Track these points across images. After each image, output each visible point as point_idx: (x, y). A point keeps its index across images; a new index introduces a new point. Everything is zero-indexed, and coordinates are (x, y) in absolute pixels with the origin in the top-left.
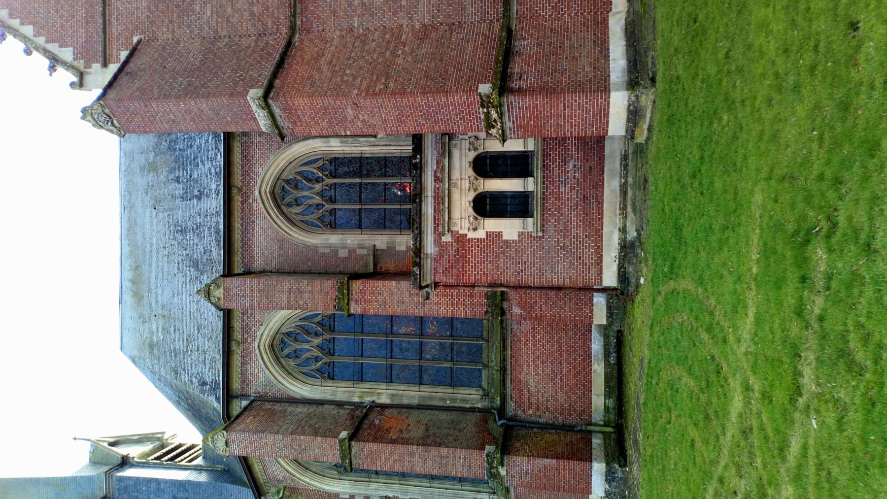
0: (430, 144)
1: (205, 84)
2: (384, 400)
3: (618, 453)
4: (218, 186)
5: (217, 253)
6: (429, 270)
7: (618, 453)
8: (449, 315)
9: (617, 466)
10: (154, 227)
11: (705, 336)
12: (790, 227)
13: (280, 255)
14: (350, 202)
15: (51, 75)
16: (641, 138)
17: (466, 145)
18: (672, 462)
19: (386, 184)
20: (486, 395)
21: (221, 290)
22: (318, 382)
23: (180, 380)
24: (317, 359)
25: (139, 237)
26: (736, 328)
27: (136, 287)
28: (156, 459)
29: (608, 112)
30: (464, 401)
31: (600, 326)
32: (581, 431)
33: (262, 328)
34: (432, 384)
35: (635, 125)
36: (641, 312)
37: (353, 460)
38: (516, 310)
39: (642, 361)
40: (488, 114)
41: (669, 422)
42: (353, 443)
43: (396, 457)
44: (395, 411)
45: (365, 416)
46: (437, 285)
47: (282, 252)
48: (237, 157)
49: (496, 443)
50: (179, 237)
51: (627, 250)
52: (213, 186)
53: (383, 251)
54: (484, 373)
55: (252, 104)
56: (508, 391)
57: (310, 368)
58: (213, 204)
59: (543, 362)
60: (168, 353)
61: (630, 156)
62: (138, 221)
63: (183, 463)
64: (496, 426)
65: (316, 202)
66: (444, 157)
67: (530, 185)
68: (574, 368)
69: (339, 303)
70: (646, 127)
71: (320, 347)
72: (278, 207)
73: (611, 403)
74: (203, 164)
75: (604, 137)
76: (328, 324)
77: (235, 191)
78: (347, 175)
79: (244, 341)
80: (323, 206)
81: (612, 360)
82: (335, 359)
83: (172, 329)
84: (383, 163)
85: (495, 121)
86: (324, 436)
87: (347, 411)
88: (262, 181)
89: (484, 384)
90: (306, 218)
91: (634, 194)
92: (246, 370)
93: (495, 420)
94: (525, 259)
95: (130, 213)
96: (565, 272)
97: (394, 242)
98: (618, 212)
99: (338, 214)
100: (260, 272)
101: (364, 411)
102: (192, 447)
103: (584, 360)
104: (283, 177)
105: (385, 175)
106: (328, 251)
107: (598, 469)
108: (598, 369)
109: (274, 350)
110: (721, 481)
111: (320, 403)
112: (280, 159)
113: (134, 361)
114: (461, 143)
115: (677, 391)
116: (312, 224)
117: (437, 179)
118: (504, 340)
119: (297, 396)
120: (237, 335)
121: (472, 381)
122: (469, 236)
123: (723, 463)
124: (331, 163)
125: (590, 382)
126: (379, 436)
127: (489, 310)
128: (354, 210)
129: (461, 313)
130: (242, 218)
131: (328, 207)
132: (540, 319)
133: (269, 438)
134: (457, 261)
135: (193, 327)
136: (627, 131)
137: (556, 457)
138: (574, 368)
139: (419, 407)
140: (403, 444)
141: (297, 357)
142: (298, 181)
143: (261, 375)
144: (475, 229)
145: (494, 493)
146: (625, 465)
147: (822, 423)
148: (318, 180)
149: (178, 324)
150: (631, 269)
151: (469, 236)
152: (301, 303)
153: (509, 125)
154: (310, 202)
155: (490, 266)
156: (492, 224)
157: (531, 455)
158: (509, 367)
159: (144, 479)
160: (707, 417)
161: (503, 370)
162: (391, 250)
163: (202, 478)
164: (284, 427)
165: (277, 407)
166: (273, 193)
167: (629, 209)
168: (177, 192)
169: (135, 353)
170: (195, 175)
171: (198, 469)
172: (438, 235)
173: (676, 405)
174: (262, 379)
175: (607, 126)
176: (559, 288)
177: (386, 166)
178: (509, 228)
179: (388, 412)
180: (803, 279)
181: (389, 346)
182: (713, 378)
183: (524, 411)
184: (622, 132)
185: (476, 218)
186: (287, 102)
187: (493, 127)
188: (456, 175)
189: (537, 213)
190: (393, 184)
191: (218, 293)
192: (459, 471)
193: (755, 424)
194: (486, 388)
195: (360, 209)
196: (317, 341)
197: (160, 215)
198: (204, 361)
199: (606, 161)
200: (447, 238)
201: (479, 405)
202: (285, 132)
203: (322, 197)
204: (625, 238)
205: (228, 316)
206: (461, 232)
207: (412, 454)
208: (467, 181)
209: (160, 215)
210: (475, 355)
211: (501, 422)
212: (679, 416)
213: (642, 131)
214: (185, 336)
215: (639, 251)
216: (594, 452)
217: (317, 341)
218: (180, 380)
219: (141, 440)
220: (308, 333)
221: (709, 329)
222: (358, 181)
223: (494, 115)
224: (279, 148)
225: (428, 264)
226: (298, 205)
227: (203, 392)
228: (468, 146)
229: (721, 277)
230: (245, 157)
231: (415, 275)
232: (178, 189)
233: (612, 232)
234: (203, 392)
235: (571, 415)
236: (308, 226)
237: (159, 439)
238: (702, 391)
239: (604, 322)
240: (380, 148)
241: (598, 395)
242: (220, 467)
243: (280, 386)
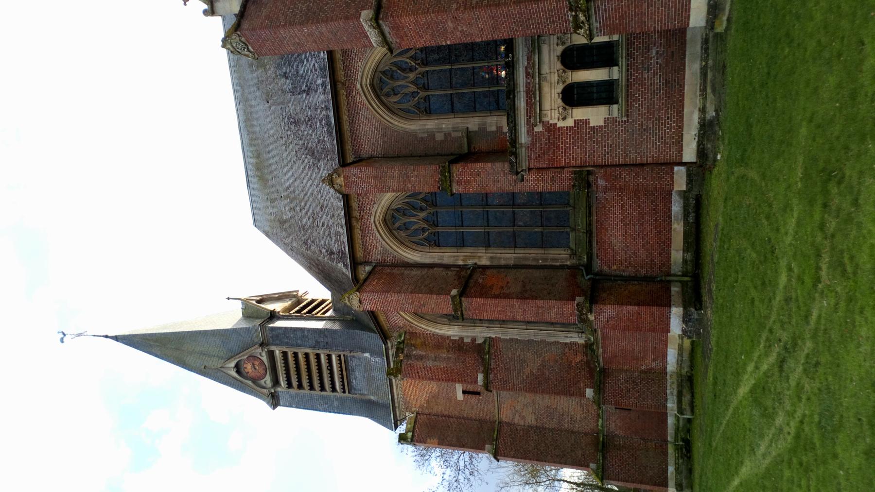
1: (322, 8)
2: (485, 262)
3: (694, 298)
4: (324, 82)
5: (331, 143)
7: (694, 298)
8: (540, 189)
9: (693, 310)
10: (269, 119)
11: (765, 221)
12: (821, 165)
13: (384, 142)
14: (441, 88)
15: (185, 4)
16: (720, 28)
17: (554, 39)
18: (738, 312)
19: (474, 68)
20: (574, 254)
21: (342, 178)
22: (427, 249)
23: (311, 251)
24: (424, 230)
25: (257, 128)
26: (785, 224)
27: (260, 171)
28: (296, 312)
29: (690, 7)
30: (553, 260)
31: (680, 193)
32: (661, 281)
33: (376, 206)
34: (525, 246)
35: (715, 17)
36: (717, 186)
38: (601, 182)
39: (717, 226)
40: (576, 17)
41: (736, 282)
42: (463, 299)
44: (495, 271)
45: (470, 276)
46: (530, 169)
49: (585, 295)
50: (294, 128)
51: (706, 128)
52: (319, 82)
53: (475, 132)
54: (572, 235)
55: (364, 25)
56: (595, 251)
58: (321, 98)
59: (626, 225)
60: (297, 229)
61: (711, 39)
62: (254, 114)
63: (319, 315)
64: (585, 280)
65: (411, 90)
66: (534, 53)
67: (615, 73)
68: (656, 228)
69: (442, 184)
70: (725, 18)
71: (425, 220)
72: (378, 97)
73: (689, 256)
74: (308, 61)
75: (686, 29)
76: (431, 200)
77: (339, 86)
78: (438, 62)
80: (418, 93)
81: (691, 219)
82: (439, 229)
83: (298, 208)
85: (583, 22)
86: (439, 294)
87: (454, 273)
89: (572, 245)
91: (714, 76)
92: (366, 242)
93: (583, 275)
94: (610, 142)
95: (245, 105)
96: (648, 151)
97: (485, 124)
98: (698, 93)
99: (432, 100)
100: (369, 158)
101: (469, 272)
102: (323, 301)
103: (664, 221)
104: (381, 68)
105: (472, 60)
107: (676, 314)
108: (678, 228)
110: (771, 331)
111: (431, 266)
113: (267, 235)
115: (743, 259)
116: (409, 111)
117: (528, 75)
118: (589, 207)
119: (411, 261)
120: (356, 213)
122: (558, 125)
123: (773, 319)
125: (670, 239)
126: (484, 292)
127: (577, 183)
128: (446, 95)
129: (551, 187)
130: (349, 111)
131: (422, 94)
132: (622, 189)
133: (394, 297)
134: (549, 148)
135: (316, 206)
136: (707, 22)
137: (638, 304)
138: (656, 228)
139: (516, 267)
140: (505, 298)
141: (406, 229)
142: (393, 71)
144: (564, 119)
145: (582, 332)
146: (701, 309)
147: (829, 304)
148: (411, 69)
149: (303, 204)
150: (709, 146)
151: (558, 125)
152: (410, 186)
153: (596, 25)
154: (406, 91)
156: (579, 113)
157: (617, 303)
158: (594, 230)
159: (291, 328)
160: (763, 283)
161: (589, 232)
162: (482, 130)
163: (329, 325)
164: (404, 288)
165: (396, 271)
167: (709, 90)
168: (287, 87)
169: (267, 228)
170: (301, 72)
171: (329, 319)
172: (531, 126)
173: (742, 269)
174: (380, 248)
175: (689, 19)
176: (642, 165)
178: (595, 115)
179: (488, 272)
180: (825, 206)
181: (485, 216)
182: (769, 256)
183: (609, 267)
184: (703, 23)
185: (564, 109)
186: (395, 21)
187: (581, 28)
188: (545, 69)
189: (622, 100)
190: (480, 67)
191: (340, 181)
192: (554, 318)
193: (794, 296)
194: (574, 248)
196: (423, 215)
197: (273, 108)
198: (330, 234)
199: (688, 46)
200: (539, 129)
201: (568, 263)
202: (393, 46)
203: (417, 85)
204: (705, 117)
205: (347, 199)
206: (551, 122)
207: (513, 306)
209: (273, 108)
212: (743, 278)
213: (722, 22)
214: (311, 214)
215: (717, 128)
216: (672, 298)
217: (423, 215)
218: (311, 251)
219: (281, 297)
220: (414, 208)
221: (768, 218)
222: (448, 67)
223: (582, 17)
225: (523, 153)
226: (395, 94)
227: (331, 259)
228: (556, 41)
229: (778, 180)
232: (287, 85)
233: (692, 112)
234: (331, 259)
235: (652, 268)
237: (294, 296)
238: (760, 262)
239: (684, 188)
241: (677, 250)
242: (349, 318)
243: (396, 254)
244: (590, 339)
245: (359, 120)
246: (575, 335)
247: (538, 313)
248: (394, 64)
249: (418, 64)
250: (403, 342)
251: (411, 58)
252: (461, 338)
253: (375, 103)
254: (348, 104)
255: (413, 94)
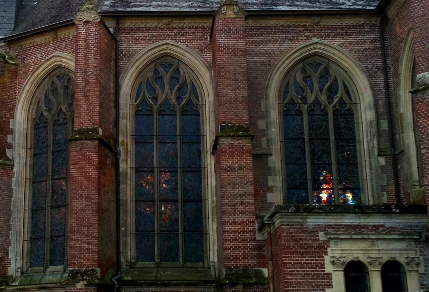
0: (408, 221)
2: (122, 166)
6: (291, 220)
13: (255, 62)
19: (330, 164)
20: (131, 265)
21: (233, 16)
24: (155, 99)
33: (184, 47)
37: (80, 142)
42: (96, 142)
43: (85, 183)
47: (259, 65)
48: (348, 21)
53: (267, 163)
57: (146, 93)
66: (399, 234)
71: (167, 101)
77: (317, 19)
78: (337, 126)
79: (171, 29)
84: (351, 162)
86: (100, 114)
88: (327, 46)
89: (140, 264)
90: (292, 88)
92: (142, 32)
97: (276, 174)
99: (298, 118)
104: (332, 65)
106: (263, 109)
109: (161, 57)
112: (350, 62)
114: (412, 250)
116: (286, 92)
117: (377, 227)
120: (176, 23)
121: (143, 253)
122: (325, 257)
124: (348, 110)
127: (233, 272)
128: (302, 133)
130: (289, 26)
131: (305, 108)
134: (301, 246)
141: (156, 79)
143: (139, 46)
144: (333, 263)
145: (22, 273)
148: (330, 99)
151: (325, 257)
152: (226, 91)
155: (300, 276)
166: (315, 54)
172: (325, 228)
177: (348, 164)
188: (382, 245)
195: (303, 139)
200: (322, 237)
202: (420, 95)
203: (314, 103)
206: (329, 250)
207: (89, 198)
208: (377, 256)
210: (169, 254)
211: (116, 282)
222: (332, 137)
224: (361, 61)
225: (297, 220)
230: (350, 29)
231: (287, 207)
236: (284, 90)
240: (367, 159)
244: (14, 281)
245: (279, 37)
246: (19, 264)
247: (81, 225)
248: (336, 80)
249: (335, 107)
250: (7, 62)
251: (341, 100)
252: (11, 132)
253: (297, 56)
254: (296, 27)
255: (304, 99)
